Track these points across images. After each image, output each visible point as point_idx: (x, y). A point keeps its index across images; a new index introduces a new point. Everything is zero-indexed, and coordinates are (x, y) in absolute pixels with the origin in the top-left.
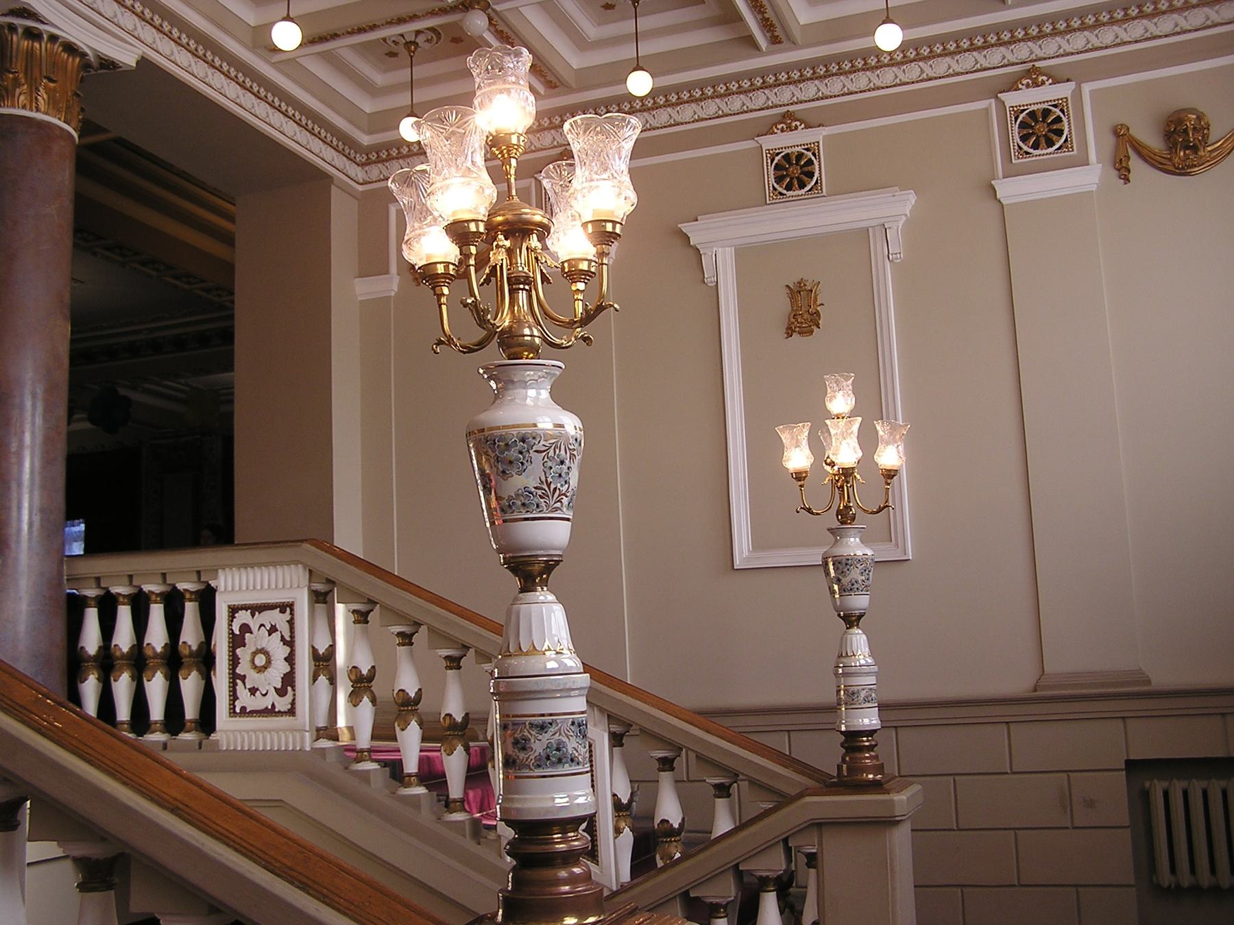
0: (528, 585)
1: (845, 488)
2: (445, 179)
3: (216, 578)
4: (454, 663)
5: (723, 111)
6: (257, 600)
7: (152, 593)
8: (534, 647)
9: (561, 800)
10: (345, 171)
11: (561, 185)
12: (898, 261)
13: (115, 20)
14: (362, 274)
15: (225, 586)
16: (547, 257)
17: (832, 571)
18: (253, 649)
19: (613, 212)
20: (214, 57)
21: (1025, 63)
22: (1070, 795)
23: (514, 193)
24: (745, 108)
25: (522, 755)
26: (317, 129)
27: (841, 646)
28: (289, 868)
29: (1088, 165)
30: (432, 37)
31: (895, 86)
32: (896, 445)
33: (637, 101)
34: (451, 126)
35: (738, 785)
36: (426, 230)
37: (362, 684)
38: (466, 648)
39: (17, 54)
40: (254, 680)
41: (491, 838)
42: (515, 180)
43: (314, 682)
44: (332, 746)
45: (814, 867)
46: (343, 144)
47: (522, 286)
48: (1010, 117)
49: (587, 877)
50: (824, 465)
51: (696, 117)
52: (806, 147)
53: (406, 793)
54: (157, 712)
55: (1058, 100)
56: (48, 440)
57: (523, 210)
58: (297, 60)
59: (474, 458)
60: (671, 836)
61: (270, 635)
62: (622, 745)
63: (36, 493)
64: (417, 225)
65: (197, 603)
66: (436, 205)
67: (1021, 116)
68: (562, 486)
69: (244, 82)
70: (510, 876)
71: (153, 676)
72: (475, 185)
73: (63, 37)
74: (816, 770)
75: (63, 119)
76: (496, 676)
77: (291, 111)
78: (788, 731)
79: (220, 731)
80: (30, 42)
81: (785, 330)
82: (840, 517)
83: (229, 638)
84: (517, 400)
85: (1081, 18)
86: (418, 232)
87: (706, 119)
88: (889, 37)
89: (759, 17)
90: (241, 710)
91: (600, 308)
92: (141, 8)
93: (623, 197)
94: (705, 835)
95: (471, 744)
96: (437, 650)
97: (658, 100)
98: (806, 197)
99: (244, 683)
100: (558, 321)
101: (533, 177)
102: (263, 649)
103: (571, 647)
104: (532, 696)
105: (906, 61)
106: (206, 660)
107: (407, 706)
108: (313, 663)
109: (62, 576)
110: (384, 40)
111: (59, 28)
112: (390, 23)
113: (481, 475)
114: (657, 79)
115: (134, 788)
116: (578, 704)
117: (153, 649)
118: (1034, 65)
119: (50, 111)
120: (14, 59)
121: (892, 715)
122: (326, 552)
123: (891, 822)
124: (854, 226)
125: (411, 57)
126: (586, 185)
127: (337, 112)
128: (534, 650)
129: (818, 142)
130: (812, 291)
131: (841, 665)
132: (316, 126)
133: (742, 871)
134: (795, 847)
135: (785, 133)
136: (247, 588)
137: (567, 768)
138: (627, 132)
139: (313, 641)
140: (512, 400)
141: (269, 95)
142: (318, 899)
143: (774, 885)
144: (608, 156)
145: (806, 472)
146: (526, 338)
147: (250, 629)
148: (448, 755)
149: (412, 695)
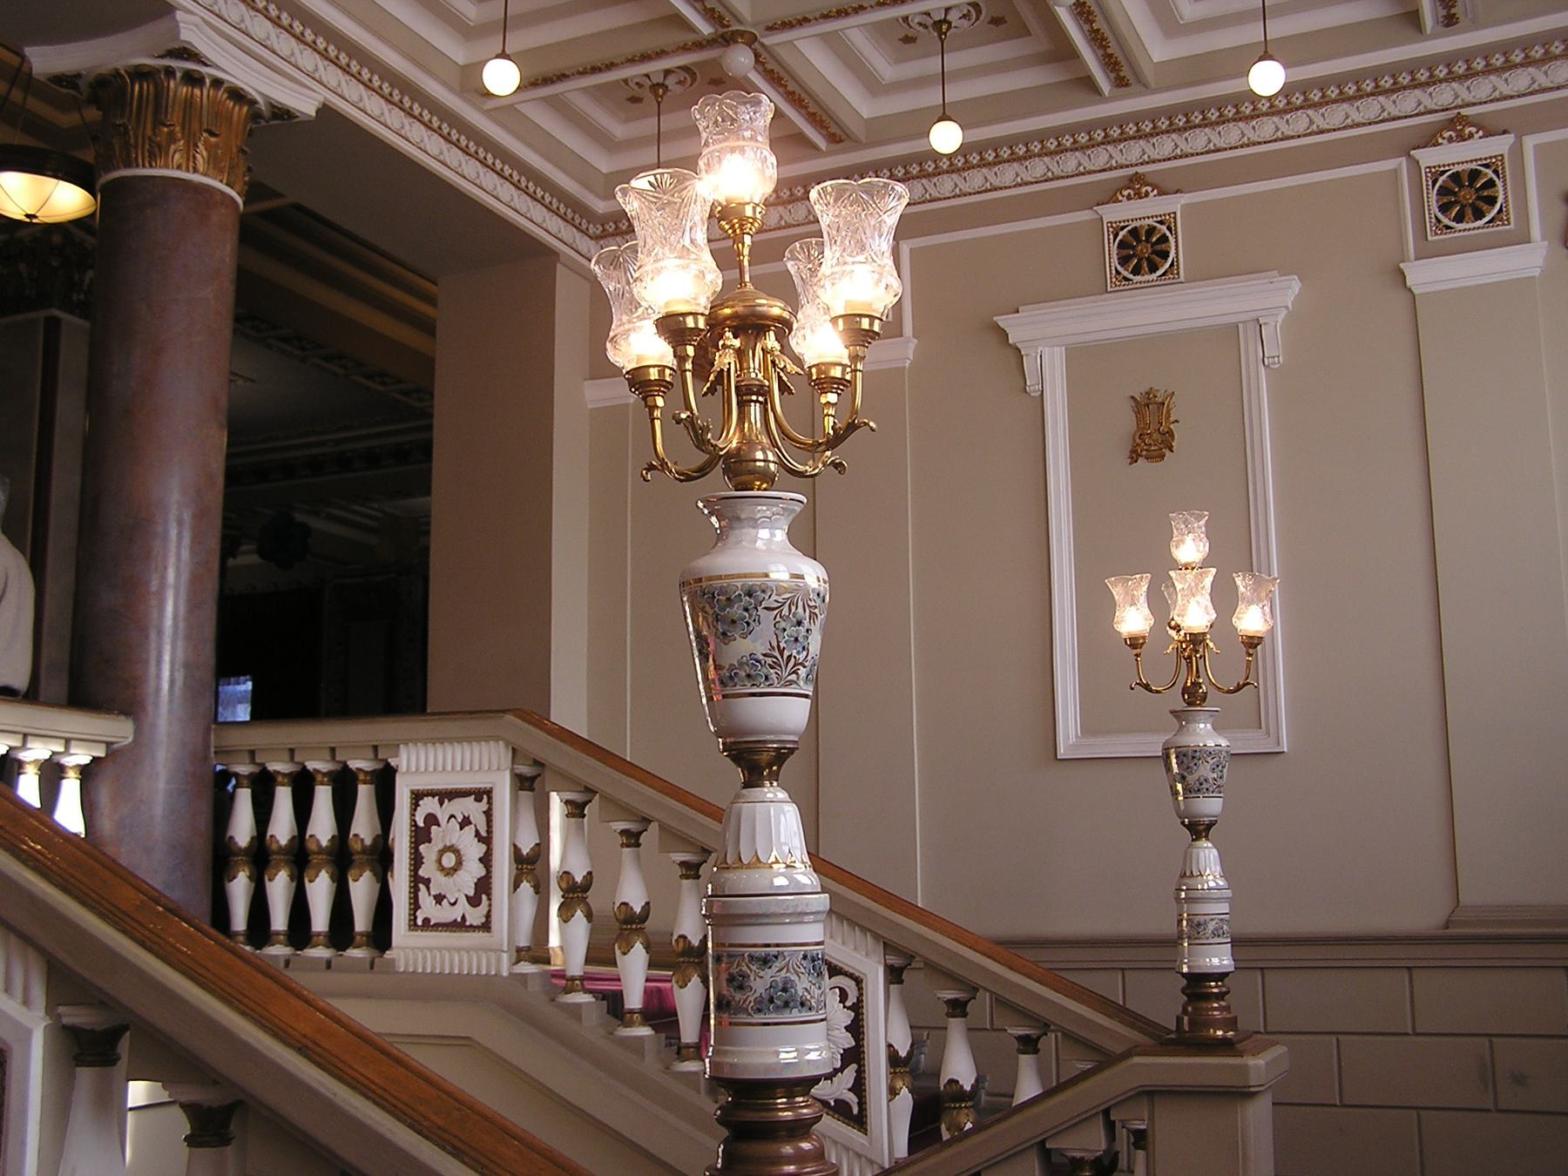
0: (753, 779)
3: (396, 755)
5: (1053, 173)
8: (758, 859)
9: (787, 1055)
10: (574, 246)
11: (810, 269)
13: (293, 60)
17: (1175, 766)
18: (441, 846)
19: (870, 305)
20: (412, 103)
21: (1447, 109)
22: (1493, 1067)
23: (747, 278)
24: (1081, 169)
25: (738, 996)
26: (540, 193)
27: (1184, 864)
28: (439, 1128)
29: (1529, 242)
30: (685, 78)
31: (1275, 141)
32: (1261, 605)
33: (944, 160)
36: (638, 324)
37: (576, 893)
39: (173, 103)
42: (750, 265)
43: (515, 890)
44: (536, 971)
45: (1143, 1148)
47: (754, 398)
48: (1426, 181)
51: (1019, 180)
52: (1159, 219)
53: (625, 1034)
54: (320, 920)
55: (1491, 158)
56: (196, 580)
57: (758, 301)
61: (461, 829)
62: (901, 982)
63: (180, 643)
64: (625, 318)
65: (373, 787)
66: (644, 293)
67: (1441, 179)
68: (798, 653)
69: (449, 134)
71: (317, 876)
72: (694, 269)
73: (228, 81)
74: (1149, 1022)
75: (225, 181)
77: (507, 171)
80: (190, 88)
83: (411, 831)
84: (743, 543)
85: (1524, 50)
86: (626, 327)
87: (1032, 183)
88: (1267, 78)
89: (1100, 52)
91: (852, 427)
96: (671, 854)
97: (1002, 153)
98: (1158, 283)
99: (428, 889)
100: (802, 443)
102: (452, 846)
103: (806, 859)
104: (752, 921)
105: (1290, 108)
106: (382, 857)
108: (515, 866)
109: (209, 747)
110: (625, 81)
112: (632, 61)
113: (696, 638)
114: (966, 132)
117: (318, 841)
118: (1459, 113)
119: (210, 172)
120: (170, 110)
123: (1244, 1094)
124: (1218, 321)
126: (837, 269)
128: (757, 863)
129: (1175, 213)
130: (1163, 404)
135: (1132, 201)
137: (796, 1015)
141: (481, 150)
145: (1144, 638)
146: (758, 464)
148: (681, 987)
149: (638, 910)
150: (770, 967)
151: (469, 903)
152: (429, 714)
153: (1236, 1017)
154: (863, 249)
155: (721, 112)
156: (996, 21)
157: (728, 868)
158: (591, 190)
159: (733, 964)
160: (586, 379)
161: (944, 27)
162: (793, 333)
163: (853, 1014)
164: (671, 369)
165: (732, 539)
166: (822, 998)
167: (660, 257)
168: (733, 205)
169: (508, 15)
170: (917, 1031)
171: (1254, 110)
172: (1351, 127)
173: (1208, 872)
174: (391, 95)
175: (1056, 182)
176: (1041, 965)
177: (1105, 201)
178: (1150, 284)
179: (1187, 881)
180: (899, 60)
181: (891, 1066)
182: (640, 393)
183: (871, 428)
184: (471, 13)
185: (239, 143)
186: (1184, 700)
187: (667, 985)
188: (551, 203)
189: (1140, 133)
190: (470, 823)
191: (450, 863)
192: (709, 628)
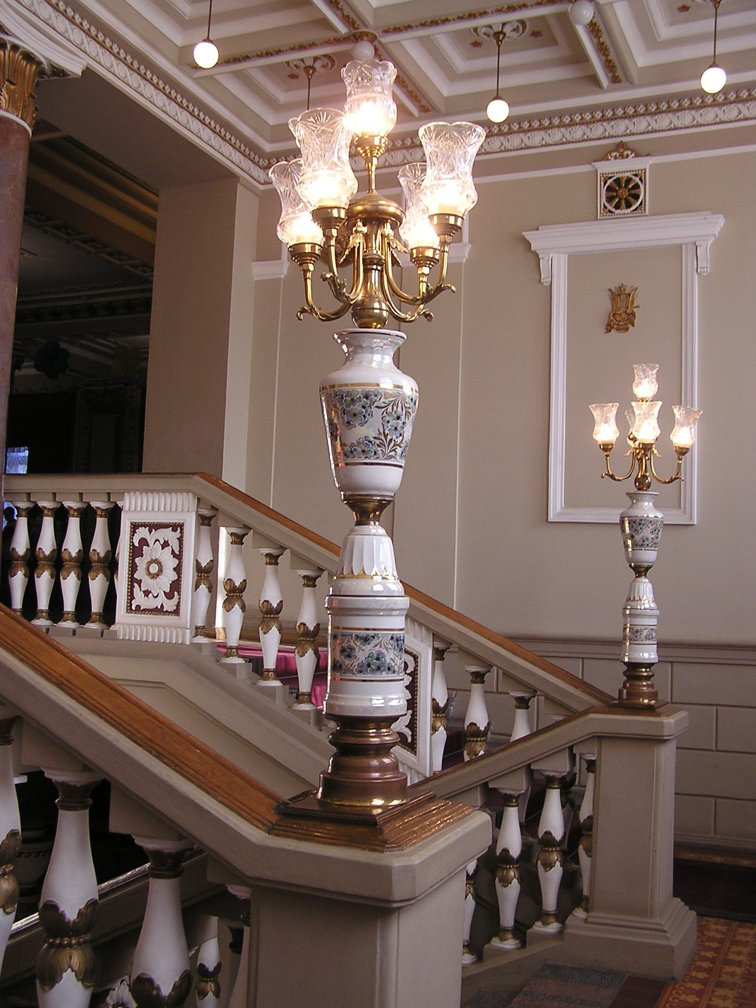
0: (363, 518)
2: (314, 171)
3: (122, 499)
4: (310, 582)
6: (154, 519)
7: (71, 508)
8: (364, 572)
9: (377, 701)
11: (415, 183)
12: (706, 274)
13: (67, 35)
14: (259, 259)
16: (398, 243)
17: (627, 529)
18: (149, 560)
23: (373, 187)
25: (347, 662)
26: (228, 136)
27: (630, 593)
30: (327, 63)
32: (689, 427)
34: (322, 125)
35: (538, 699)
36: (298, 215)
37: (235, 593)
41: (331, 726)
43: (196, 589)
44: (207, 642)
45: (593, 772)
50: (628, 439)
52: (634, 173)
54: (69, 604)
57: (380, 202)
58: (215, 77)
60: (478, 736)
61: (163, 549)
62: (443, 659)
64: (290, 210)
65: (106, 519)
68: (397, 437)
71: (68, 576)
72: (339, 177)
73: (23, 47)
74: (601, 692)
76: (331, 593)
78: (583, 658)
79: (118, 623)
81: (605, 327)
82: (637, 484)
83: (130, 549)
84: (364, 363)
86: (291, 216)
89: (595, 41)
90: (136, 607)
91: (439, 289)
93: (465, 195)
96: (298, 571)
99: (140, 587)
100: (403, 298)
102: (157, 559)
103: (396, 574)
105: (727, 102)
106: (110, 565)
110: (288, 63)
111: (20, 40)
112: (293, 49)
113: (329, 425)
114: (511, 109)
116: (398, 622)
119: (10, 109)
121: (667, 652)
123: (660, 741)
125: (309, 80)
126: (435, 182)
130: (630, 295)
131: (629, 607)
132: (228, 134)
133: (533, 770)
137: (385, 675)
138: (473, 139)
139: (197, 555)
140: (361, 362)
142: (171, 767)
143: (559, 784)
144: (455, 159)
145: (612, 445)
148: (301, 656)
149: (275, 605)
150: (369, 644)
151: (166, 596)
152: (144, 474)
153: (657, 692)
154: (453, 170)
155: (361, 73)
156: (535, 34)
157: (344, 578)
158: (262, 136)
159: (344, 641)
160: (253, 261)
161: (501, 37)
162: (402, 226)
163: (411, 678)
164: (320, 246)
165: (356, 360)
167: (317, 168)
168: (366, 137)
170: (450, 692)
171: (702, 102)
173: (645, 598)
176: (535, 653)
178: (626, 216)
179: (631, 603)
180: (469, 58)
181: (434, 713)
182: (298, 261)
183: (452, 290)
184: (187, 10)
186: (636, 486)
187: (292, 655)
188: (235, 143)
189: (626, 115)
190: (169, 545)
191: (155, 567)
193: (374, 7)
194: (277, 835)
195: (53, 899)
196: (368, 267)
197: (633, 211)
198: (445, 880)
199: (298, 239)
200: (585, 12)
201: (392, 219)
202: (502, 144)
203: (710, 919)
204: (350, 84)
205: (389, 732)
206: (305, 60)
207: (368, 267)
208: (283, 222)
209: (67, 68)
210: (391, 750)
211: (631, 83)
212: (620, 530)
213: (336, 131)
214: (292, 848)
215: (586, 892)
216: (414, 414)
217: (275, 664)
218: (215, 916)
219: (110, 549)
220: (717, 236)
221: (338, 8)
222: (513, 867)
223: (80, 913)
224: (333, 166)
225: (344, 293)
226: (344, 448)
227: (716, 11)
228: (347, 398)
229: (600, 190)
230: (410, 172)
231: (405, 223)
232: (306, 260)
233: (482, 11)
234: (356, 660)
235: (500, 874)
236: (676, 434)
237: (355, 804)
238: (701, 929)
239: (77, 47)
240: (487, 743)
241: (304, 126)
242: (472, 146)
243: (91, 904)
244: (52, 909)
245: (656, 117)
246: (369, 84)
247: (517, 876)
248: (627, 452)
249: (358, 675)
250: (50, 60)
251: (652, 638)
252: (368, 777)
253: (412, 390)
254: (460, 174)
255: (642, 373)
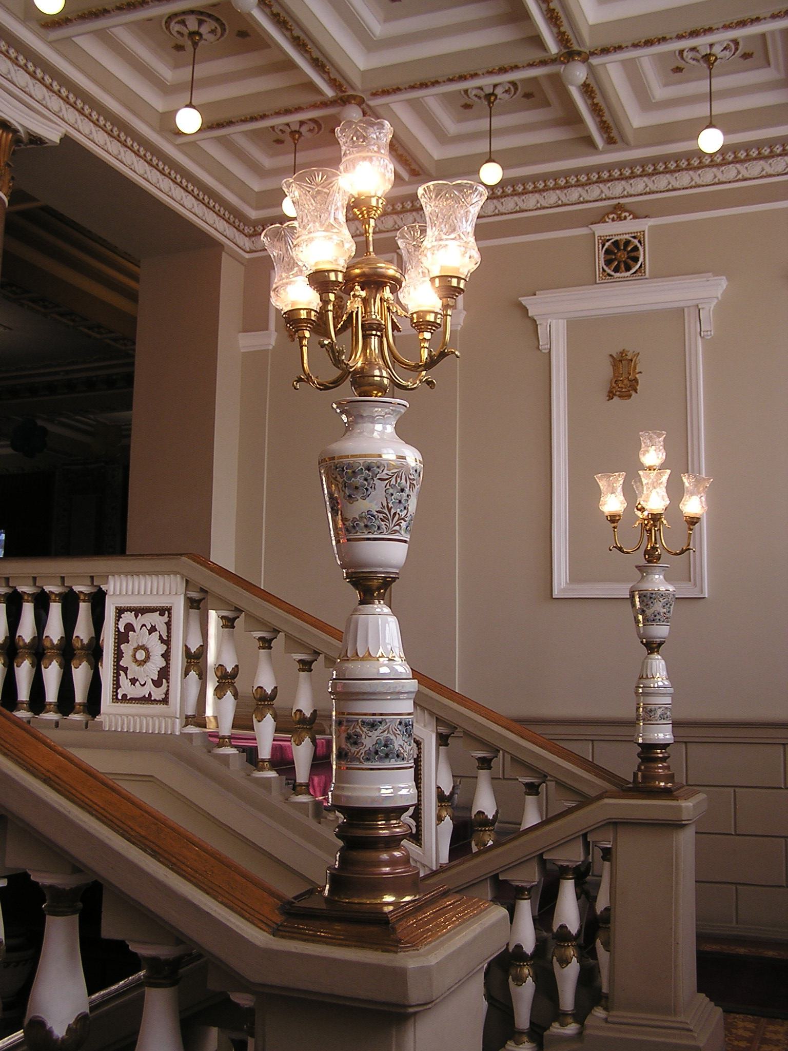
0: (367, 597)
1: (653, 531)
2: (310, 233)
3: (106, 583)
4: (306, 666)
5: (562, 201)
8: (369, 653)
9: (386, 791)
11: (414, 245)
12: (709, 337)
13: (44, 103)
15: (126, 591)
17: (638, 603)
18: (135, 646)
23: (371, 249)
25: (354, 749)
27: (642, 670)
32: (699, 496)
34: (317, 185)
35: (547, 785)
37: (226, 680)
38: (317, 653)
40: (135, 671)
41: (331, 819)
43: (186, 676)
45: (608, 860)
46: (234, 217)
47: (374, 332)
49: (406, 860)
50: (636, 510)
52: (633, 235)
54: (52, 694)
55: (637, 232)
57: (379, 265)
58: (197, 142)
59: (324, 483)
61: (150, 634)
62: (447, 745)
64: (284, 275)
65: (90, 604)
66: (301, 256)
68: (401, 511)
70: (338, 856)
71: (50, 664)
74: (614, 776)
76: (334, 677)
79: (104, 714)
81: (607, 394)
82: (647, 557)
83: (115, 635)
84: (365, 433)
87: (547, 208)
89: (589, 102)
90: (122, 697)
91: (443, 355)
92: (66, 93)
93: (467, 255)
94: (513, 826)
95: (317, 737)
98: (631, 278)
99: (126, 675)
100: (406, 365)
101: (396, 252)
103: (402, 655)
105: (725, 163)
106: (95, 653)
107: (264, 701)
110: (273, 128)
112: (278, 114)
113: (330, 499)
115: (12, 758)
116: (406, 706)
121: (682, 731)
122: (201, 565)
123: (678, 825)
125: (296, 144)
126: (435, 243)
127: (232, 191)
128: (369, 656)
129: (644, 231)
130: (632, 360)
132: (211, 201)
133: (546, 860)
134: (593, 842)
136: (133, 593)
137: (393, 763)
138: (475, 198)
139: (186, 641)
140: (361, 433)
142: (168, 867)
143: (573, 874)
145: (619, 516)
146: (376, 378)
147: (134, 628)
148: (297, 745)
149: (269, 692)
154: (454, 230)
156: (528, 96)
157: (348, 660)
160: (240, 332)
161: (492, 98)
162: (401, 290)
164: (316, 311)
166: (411, 752)
169: (195, 78)
170: (455, 778)
172: (765, 177)
174: (112, 131)
175: (564, 207)
176: (544, 736)
177: (597, 221)
178: (625, 279)
179: (644, 681)
180: (460, 121)
181: (439, 802)
182: (293, 328)
183: (456, 355)
185: (6, 159)
186: (646, 559)
187: (288, 743)
190: (156, 630)
191: (142, 656)
192: (339, 491)
193: (361, 69)
194: (283, 937)
195: (43, 1016)
196: (367, 332)
197: (633, 274)
198: (462, 981)
199: (293, 305)
200: (578, 73)
201: (391, 282)
202: (496, 208)
203: (737, 1016)
204: (344, 144)
205: (399, 823)
206: (290, 124)
207: (367, 332)
208: (277, 287)
209: (45, 136)
210: (402, 842)
211: (627, 144)
212: (630, 606)
213: (331, 191)
214: (299, 951)
215: (605, 990)
216: (418, 486)
217: (270, 753)
218: (215, 1026)
219: (94, 635)
220: (720, 298)
221: (325, 72)
222: (527, 965)
223: (69, 1030)
224: (330, 227)
225: (343, 360)
226: (346, 523)
227: (710, 72)
228: (348, 471)
229: (599, 253)
230: (409, 233)
231: (405, 287)
232: (301, 326)
233: (472, 73)
234: (362, 748)
235: (513, 971)
236: (685, 503)
237: (364, 901)
238: (728, 1027)
239: (55, 114)
240: (495, 832)
241: (298, 187)
242: (473, 206)
243: (82, 1019)
244: (39, 1025)
245: (654, 178)
246: (364, 143)
247: (531, 974)
248: (635, 524)
249: (365, 763)
250: (27, 128)
251: (667, 717)
252: (379, 872)
253: (416, 461)
254: (462, 235)
255: (648, 441)
